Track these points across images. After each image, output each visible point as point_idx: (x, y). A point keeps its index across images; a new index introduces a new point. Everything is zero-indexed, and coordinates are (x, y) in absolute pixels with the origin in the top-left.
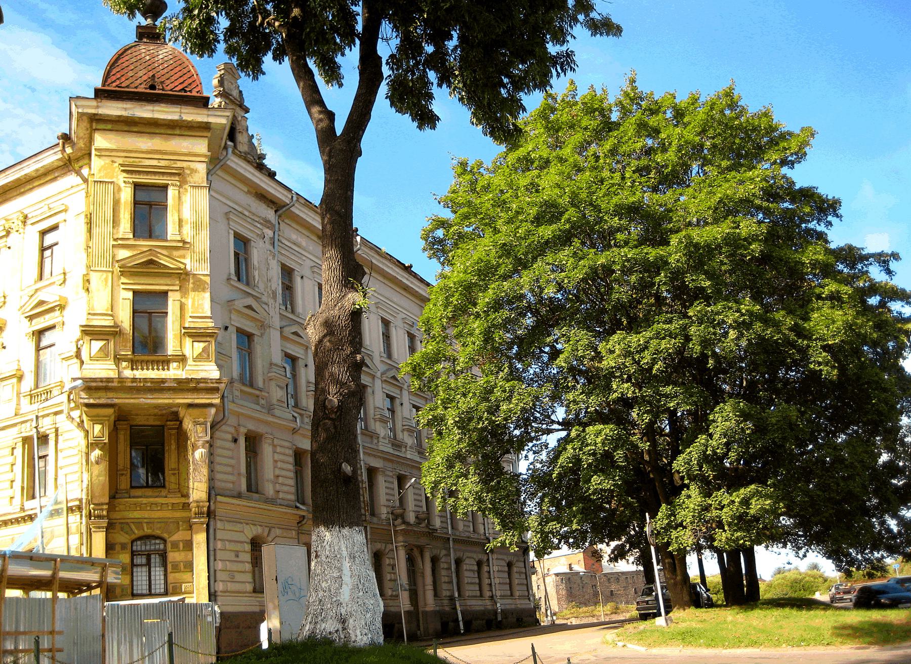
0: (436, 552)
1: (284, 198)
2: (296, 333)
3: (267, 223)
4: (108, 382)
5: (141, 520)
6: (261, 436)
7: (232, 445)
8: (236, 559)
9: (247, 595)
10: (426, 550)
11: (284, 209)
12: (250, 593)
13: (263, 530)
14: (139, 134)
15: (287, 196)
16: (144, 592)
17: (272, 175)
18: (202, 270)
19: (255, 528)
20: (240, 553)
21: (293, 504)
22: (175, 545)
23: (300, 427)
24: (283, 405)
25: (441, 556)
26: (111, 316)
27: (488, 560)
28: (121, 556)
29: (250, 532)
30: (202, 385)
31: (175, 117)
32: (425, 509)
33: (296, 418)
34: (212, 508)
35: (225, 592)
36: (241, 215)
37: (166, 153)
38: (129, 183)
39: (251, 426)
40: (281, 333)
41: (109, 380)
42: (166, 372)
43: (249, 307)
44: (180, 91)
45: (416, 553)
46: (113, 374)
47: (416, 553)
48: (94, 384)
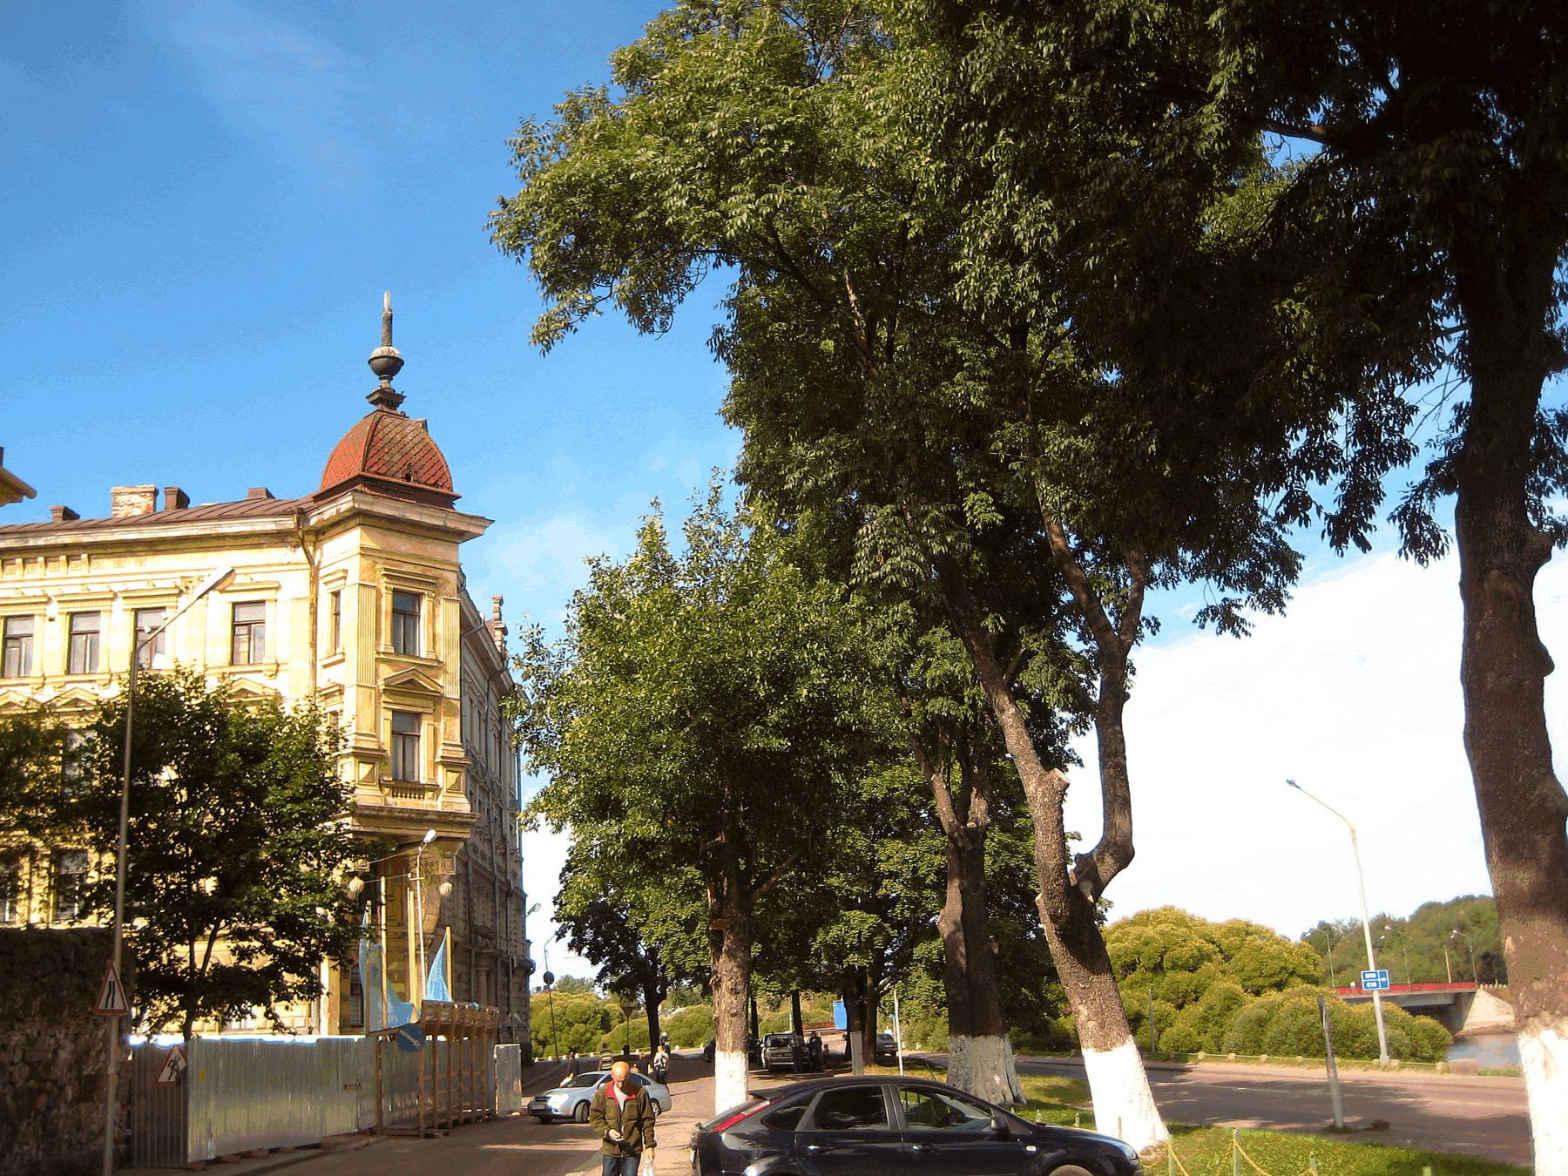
18: (452, 691)
30: (458, 819)
31: (440, 523)
42: (420, 802)
46: (379, 802)
48: (366, 812)
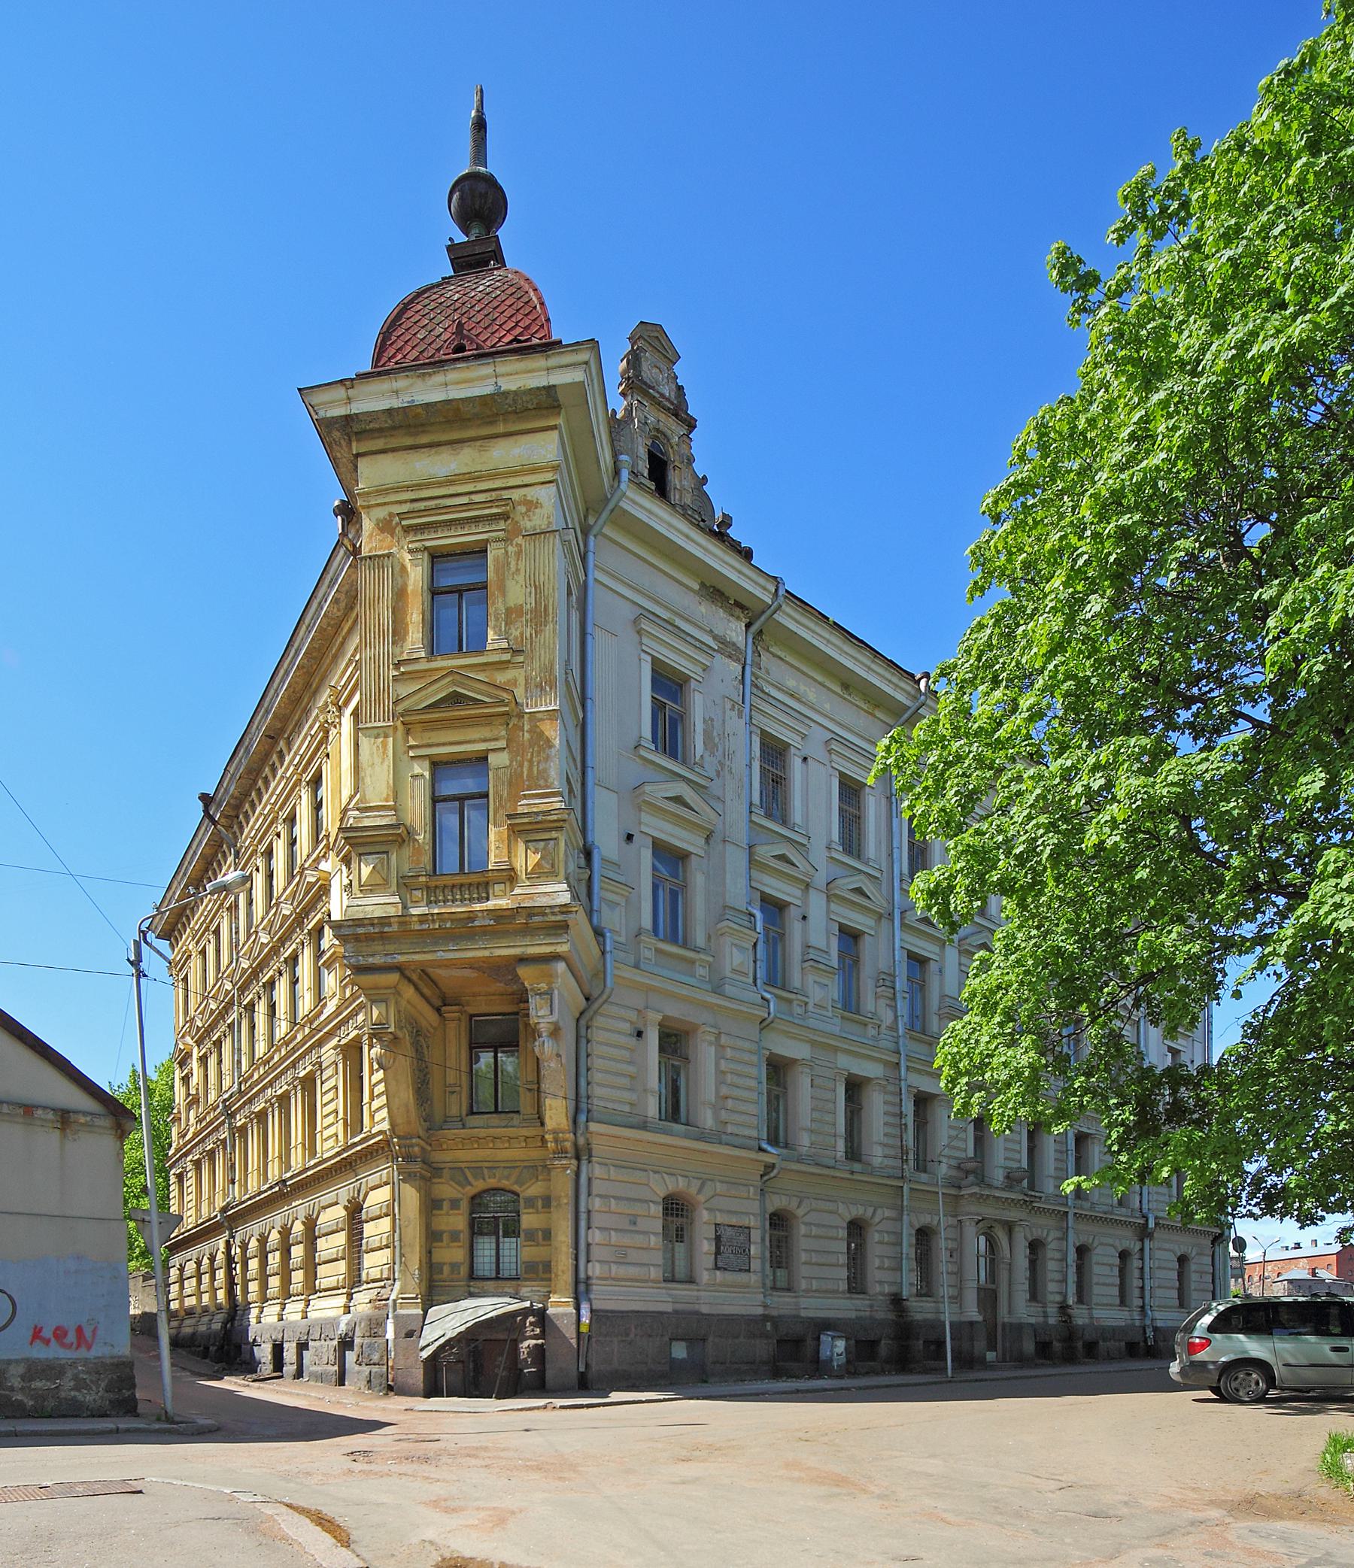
0: (1037, 1233)
1: (758, 592)
2: (859, 891)
3: (727, 648)
4: (382, 925)
5: (479, 1164)
6: (695, 1028)
7: (633, 1041)
8: (633, 1228)
9: (650, 1284)
10: (1017, 1229)
11: (763, 618)
12: (658, 1282)
13: (689, 1185)
14: (433, 450)
15: (765, 589)
16: (487, 1274)
17: (747, 555)
19: (673, 1178)
20: (639, 1220)
21: (755, 1144)
22: (531, 1202)
23: (775, 1017)
24: (744, 979)
25: (1193, 1255)
26: (393, 808)
27: (1142, 1250)
28: (452, 1219)
29: (661, 1187)
32: (1025, 1164)
33: (767, 1001)
34: (581, 1141)
35: (605, 1279)
36: (670, 627)
37: (479, 478)
38: (417, 550)
39: (674, 1010)
40: (751, 855)
41: (384, 921)
43: (859, 891)
44: (510, 342)
45: (1001, 1235)
47: (1001, 1235)
48: (361, 931)
